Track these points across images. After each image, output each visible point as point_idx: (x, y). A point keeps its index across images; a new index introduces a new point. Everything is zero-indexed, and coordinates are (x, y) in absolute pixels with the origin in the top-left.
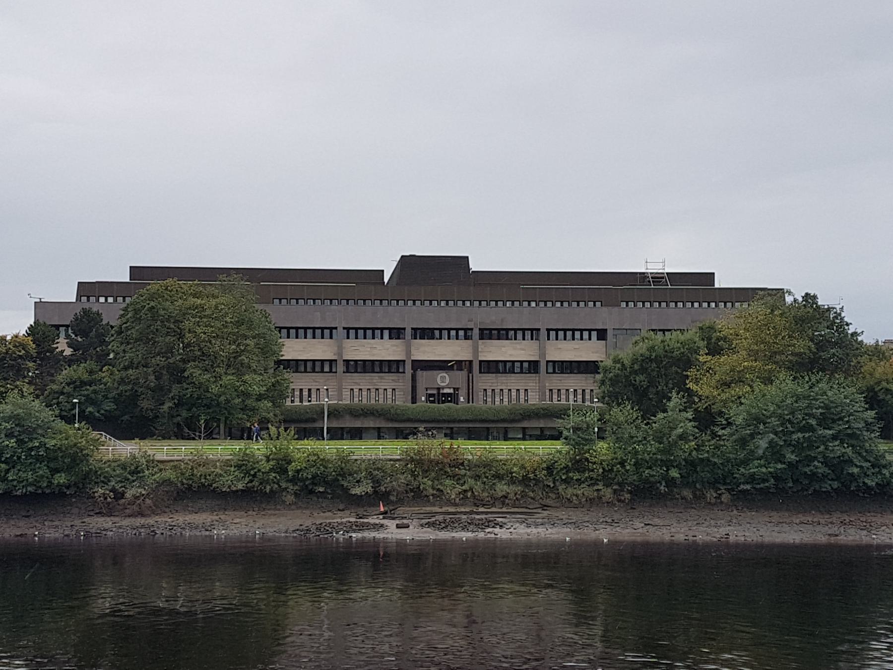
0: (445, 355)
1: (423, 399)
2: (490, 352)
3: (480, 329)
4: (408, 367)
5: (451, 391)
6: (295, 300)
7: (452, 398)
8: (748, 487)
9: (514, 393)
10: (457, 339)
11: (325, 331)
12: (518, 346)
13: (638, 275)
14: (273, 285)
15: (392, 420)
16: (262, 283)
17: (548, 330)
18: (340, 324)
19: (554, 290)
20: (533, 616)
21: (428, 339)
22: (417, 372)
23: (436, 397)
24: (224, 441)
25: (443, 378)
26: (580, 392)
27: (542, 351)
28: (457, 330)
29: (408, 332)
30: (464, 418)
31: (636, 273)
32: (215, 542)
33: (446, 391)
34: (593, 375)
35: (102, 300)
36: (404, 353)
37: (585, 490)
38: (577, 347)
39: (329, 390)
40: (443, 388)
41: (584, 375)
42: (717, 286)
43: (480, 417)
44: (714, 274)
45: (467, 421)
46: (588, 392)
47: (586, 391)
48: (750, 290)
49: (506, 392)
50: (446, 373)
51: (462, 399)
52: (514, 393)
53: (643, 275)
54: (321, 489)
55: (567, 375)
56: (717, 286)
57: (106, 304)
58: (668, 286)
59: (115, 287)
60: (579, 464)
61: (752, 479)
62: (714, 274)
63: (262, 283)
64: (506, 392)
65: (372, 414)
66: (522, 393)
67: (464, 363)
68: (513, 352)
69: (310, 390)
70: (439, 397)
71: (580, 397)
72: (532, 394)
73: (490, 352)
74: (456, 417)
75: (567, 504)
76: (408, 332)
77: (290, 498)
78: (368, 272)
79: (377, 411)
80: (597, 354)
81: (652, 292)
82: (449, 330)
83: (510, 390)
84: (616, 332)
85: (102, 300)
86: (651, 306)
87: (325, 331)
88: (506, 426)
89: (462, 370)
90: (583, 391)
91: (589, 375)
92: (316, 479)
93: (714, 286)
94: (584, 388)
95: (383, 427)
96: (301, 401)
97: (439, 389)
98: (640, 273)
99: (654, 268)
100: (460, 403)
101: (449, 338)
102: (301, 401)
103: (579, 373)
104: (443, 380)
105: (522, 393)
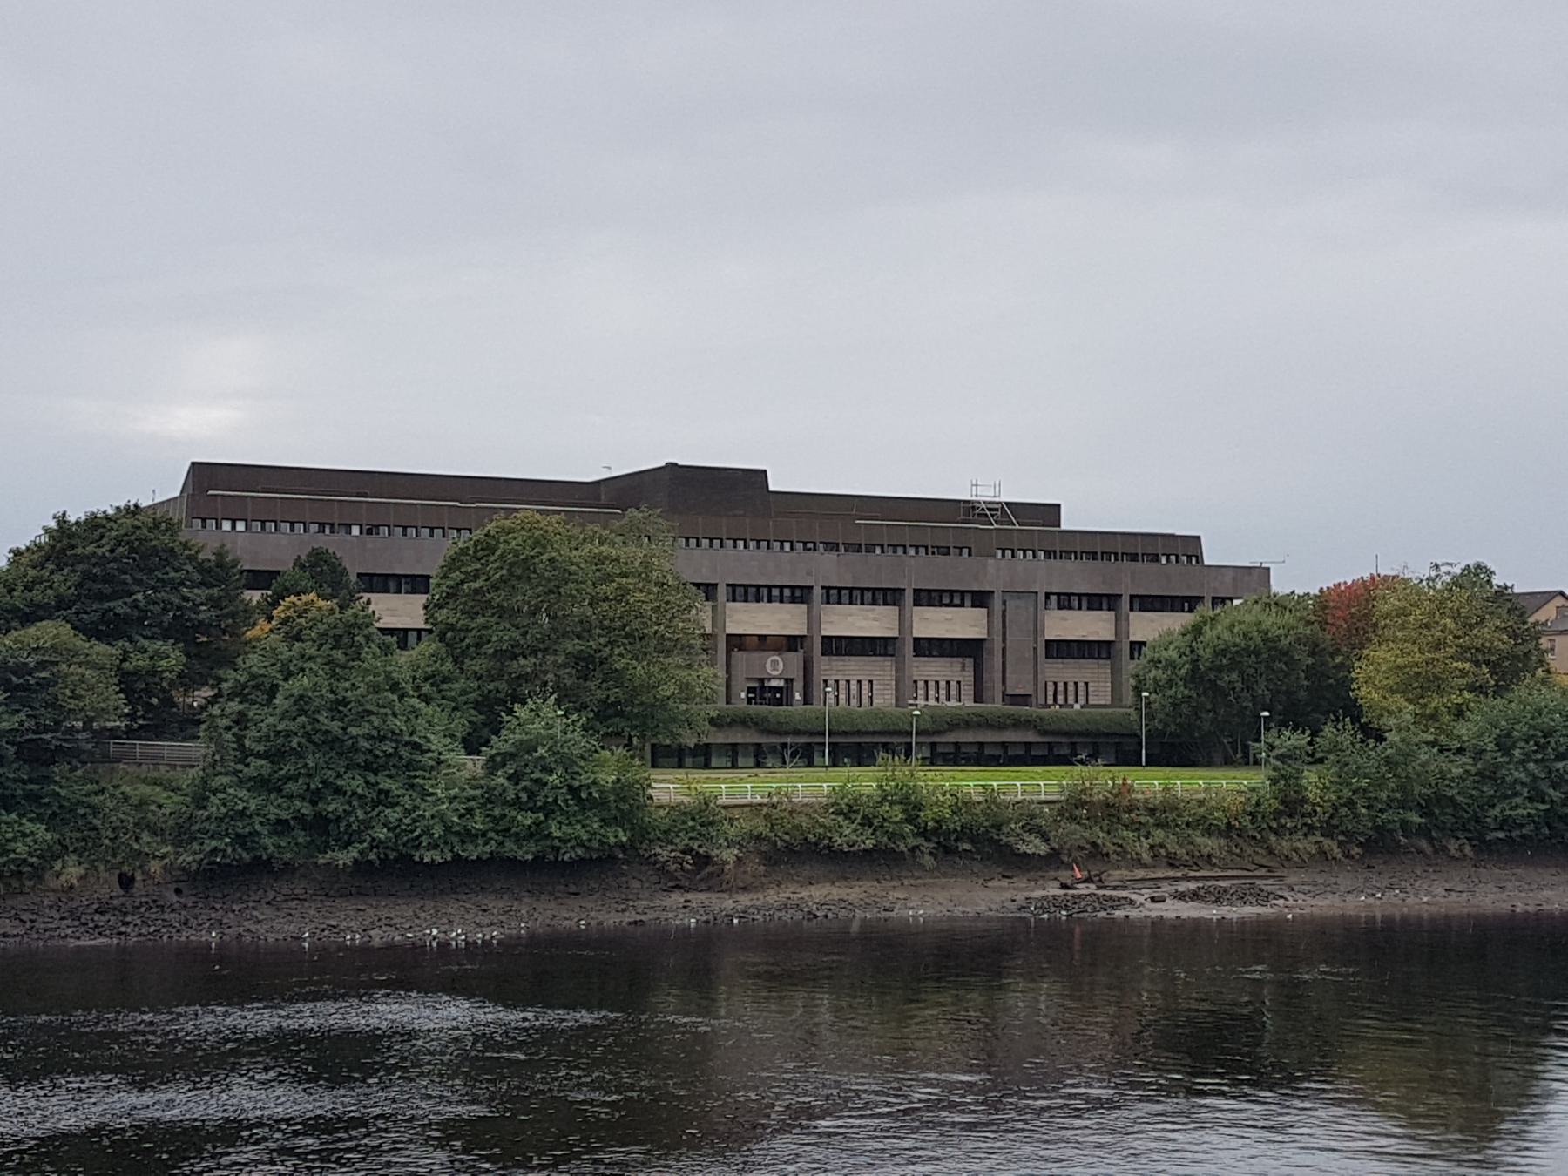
0: (769, 626)
1: (743, 695)
2: (831, 622)
3: (915, 590)
4: (722, 646)
5: (781, 683)
6: (200, 521)
7: (781, 696)
8: (1501, 835)
9: (854, 687)
10: (781, 601)
11: (843, 592)
12: (871, 615)
13: (962, 505)
14: (590, 512)
15: (770, 732)
16: (210, 492)
17: (1048, 595)
18: (1126, 589)
19: (364, 505)
20: (60, 1105)
21: (1140, 610)
22: (733, 654)
23: (785, 691)
24: (782, 770)
25: (775, 663)
26: (943, 684)
27: (812, 620)
28: (781, 588)
29: (818, 593)
30: (871, 728)
31: (959, 501)
32: (1064, 927)
33: (774, 683)
34: (960, 659)
35: (227, 526)
36: (986, 631)
37: (1306, 845)
38: (949, 616)
39: (1090, 684)
40: (769, 679)
41: (948, 659)
42: (1064, 526)
43: (891, 728)
44: (1059, 506)
45: (874, 733)
46: (953, 684)
47: (952, 683)
48: (1179, 540)
49: (842, 684)
50: (779, 655)
51: (797, 696)
52: (854, 687)
53: (967, 505)
54: (967, 847)
55: (926, 659)
56: (1064, 526)
57: (233, 533)
58: (1014, 525)
59: (1139, 539)
60: (1292, 804)
61: (1503, 824)
62: (1059, 506)
63: (210, 492)
64: (842, 684)
65: (979, 725)
66: (865, 686)
67: (799, 639)
68: (864, 624)
69: (1076, 683)
70: (760, 692)
71: (943, 692)
72: (878, 687)
73: (831, 622)
74: (860, 727)
75: (1286, 863)
76: (818, 593)
77: (928, 861)
78: (789, 496)
79: (752, 719)
80: (976, 629)
81: (279, 504)
82: (770, 587)
83: (848, 682)
84: (1007, 597)
85: (227, 526)
86: (276, 529)
87: (843, 592)
88: (981, 739)
89: (796, 651)
90: (948, 683)
91: (955, 659)
92: (965, 832)
93: (1059, 526)
94: (949, 679)
95: (1014, 743)
96: (948, 699)
97: (762, 680)
98: (965, 501)
99: (985, 494)
100: (794, 702)
101: (770, 601)
102: (927, 699)
103: (941, 655)
104: (775, 668)
105: (865, 686)
